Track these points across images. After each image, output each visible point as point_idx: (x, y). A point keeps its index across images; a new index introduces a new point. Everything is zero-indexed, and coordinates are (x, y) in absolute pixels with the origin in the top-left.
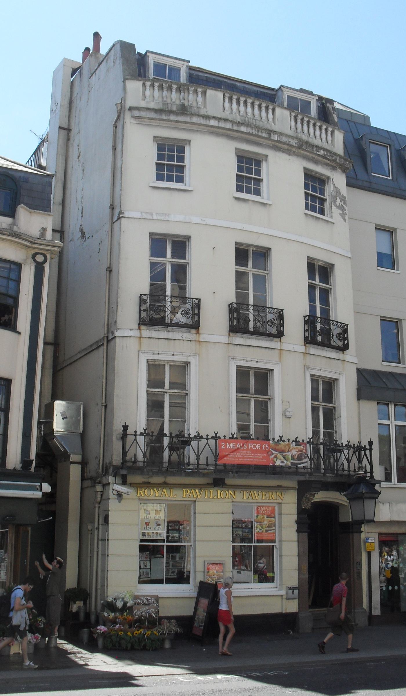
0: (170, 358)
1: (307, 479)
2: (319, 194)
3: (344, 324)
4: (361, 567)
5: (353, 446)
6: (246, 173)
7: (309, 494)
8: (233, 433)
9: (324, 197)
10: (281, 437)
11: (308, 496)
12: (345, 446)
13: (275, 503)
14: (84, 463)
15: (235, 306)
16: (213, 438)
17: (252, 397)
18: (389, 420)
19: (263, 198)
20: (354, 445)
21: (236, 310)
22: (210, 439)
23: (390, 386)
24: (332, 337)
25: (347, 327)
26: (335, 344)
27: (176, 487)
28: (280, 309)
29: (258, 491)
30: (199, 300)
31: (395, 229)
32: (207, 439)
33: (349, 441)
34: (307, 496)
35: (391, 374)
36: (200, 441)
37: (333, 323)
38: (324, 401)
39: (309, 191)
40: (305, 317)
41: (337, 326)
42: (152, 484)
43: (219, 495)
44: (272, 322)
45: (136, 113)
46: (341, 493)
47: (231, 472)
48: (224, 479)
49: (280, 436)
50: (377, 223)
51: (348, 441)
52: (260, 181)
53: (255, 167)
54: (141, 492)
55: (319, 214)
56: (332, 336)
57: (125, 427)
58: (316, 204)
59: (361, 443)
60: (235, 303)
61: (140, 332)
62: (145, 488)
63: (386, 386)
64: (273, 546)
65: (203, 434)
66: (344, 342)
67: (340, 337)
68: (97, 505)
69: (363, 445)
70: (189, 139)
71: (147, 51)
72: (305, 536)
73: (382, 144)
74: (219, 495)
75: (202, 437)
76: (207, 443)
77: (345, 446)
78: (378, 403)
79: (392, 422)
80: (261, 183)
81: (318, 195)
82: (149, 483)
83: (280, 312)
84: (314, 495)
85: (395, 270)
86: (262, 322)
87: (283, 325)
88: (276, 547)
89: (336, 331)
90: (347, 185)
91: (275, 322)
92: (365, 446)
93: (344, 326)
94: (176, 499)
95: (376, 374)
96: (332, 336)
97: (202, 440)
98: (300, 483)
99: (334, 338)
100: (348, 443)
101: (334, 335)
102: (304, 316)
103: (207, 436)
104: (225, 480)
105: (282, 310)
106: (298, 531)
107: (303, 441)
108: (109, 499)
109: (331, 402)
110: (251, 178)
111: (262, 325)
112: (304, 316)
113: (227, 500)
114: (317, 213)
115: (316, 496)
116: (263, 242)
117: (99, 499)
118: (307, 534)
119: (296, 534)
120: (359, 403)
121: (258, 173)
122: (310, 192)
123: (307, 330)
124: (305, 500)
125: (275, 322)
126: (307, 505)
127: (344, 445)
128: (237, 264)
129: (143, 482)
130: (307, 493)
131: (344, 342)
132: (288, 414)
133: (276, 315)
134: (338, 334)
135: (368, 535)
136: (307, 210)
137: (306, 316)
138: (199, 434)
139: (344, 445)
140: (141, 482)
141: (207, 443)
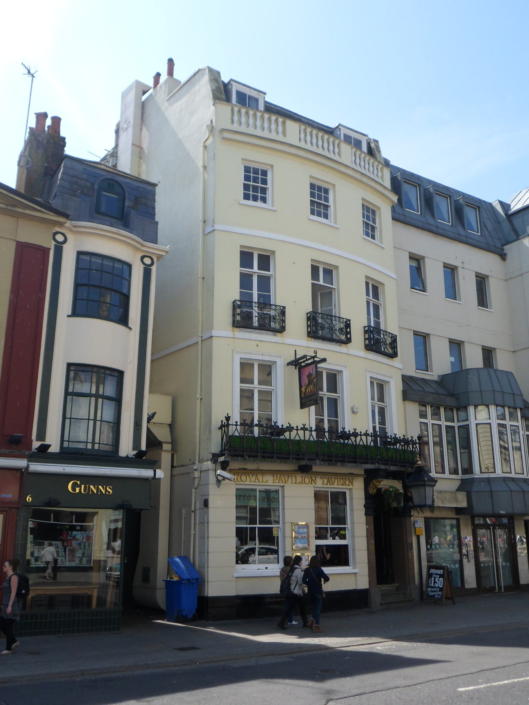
0: (260, 358)
1: (377, 467)
2: (317, 199)
3: (393, 334)
4: (412, 548)
5: (359, 433)
6: (253, 182)
7: (376, 481)
8: (304, 424)
9: (374, 225)
10: (304, 425)
11: (375, 483)
12: (352, 433)
13: (348, 488)
14: (174, 451)
15: (239, 303)
16: (302, 429)
17: (325, 395)
18: (441, 421)
19: (331, 222)
20: (391, 436)
21: (240, 307)
22: (300, 430)
23: (426, 390)
24: (334, 332)
25: (350, 322)
26: (338, 338)
27: (267, 473)
28: (282, 307)
29: (288, 476)
30: (284, 307)
31: (423, 258)
32: (297, 430)
33: (356, 429)
34: (374, 483)
35: (423, 379)
36: (292, 431)
37: (335, 319)
38: (328, 391)
39: (322, 201)
40: (365, 327)
41: (339, 321)
42: (249, 470)
43: (303, 481)
44: (341, 330)
45: (227, 135)
46: (399, 481)
47: (318, 460)
48: (312, 466)
49: (303, 424)
50: (411, 251)
51: (343, 428)
52: (327, 206)
53: (325, 195)
54: (238, 478)
55: (317, 216)
56: (334, 330)
57: (228, 418)
58: (321, 209)
59: (345, 428)
60: (238, 301)
61: (234, 333)
62: (241, 474)
63: (424, 390)
64: (345, 527)
65: (294, 425)
66: (347, 337)
67: (343, 331)
68: (193, 491)
69: (414, 439)
70: (272, 164)
71: (231, 80)
72: (371, 518)
73: (445, 195)
74: (303, 481)
75: (293, 428)
76: (297, 433)
77: (352, 433)
78: (419, 404)
79: (429, 421)
80: (329, 209)
81: (323, 202)
82: (245, 469)
83: (283, 309)
84: (380, 483)
85: (456, 300)
86: (335, 330)
87: (350, 333)
88: (348, 530)
89: (338, 325)
90: (392, 219)
91: (277, 317)
92: (416, 440)
93: (346, 322)
94: (268, 484)
95: (411, 378)
96: (334, 330)
97: (293, 430)
98: (366, 471)
99: (337, 332)
100: (355, 431)
101: (336, 330)
102: (364, 327)
103: (297, 427)
104: (313, 467)
105: (349, 320)
106: (366, 514)
107: (361, 432)
108: (209, 484)
109: (336, 392)
110: (321, 204)
111: (386, 346)
112: (364, 327)
113: (310, 485)
114: (321, 217)
115: (382, 483)
116: (331, 261)
117: (196, 485)
118: (372, 517)
119: (364, 517)
120: (404, 403)
121: (327, 199)
122: (316, 200)
123: (367, 339)
124: (372, 486)
125: (344, 330)
126: (373, 491)
127: (351, 433)
128: (313, 279)
129: (239, 468)
130: (374, 480)
131: (394, 350)
132: (355, 410)
133: (345, 324)
134: (340, 328)
135: (416, 519)
136: (313, 215)
137: (366, 327)
138: (290, 425)
139: (351, 433)
140: (238, 469)
141: (297, 433)
